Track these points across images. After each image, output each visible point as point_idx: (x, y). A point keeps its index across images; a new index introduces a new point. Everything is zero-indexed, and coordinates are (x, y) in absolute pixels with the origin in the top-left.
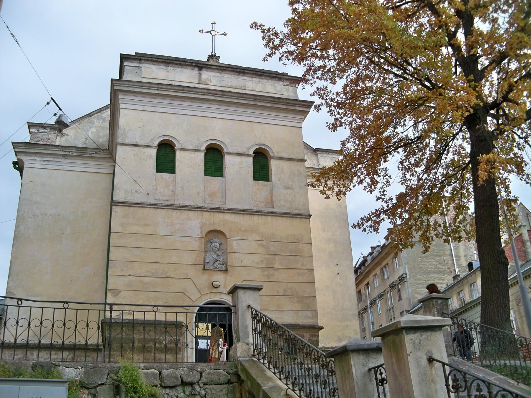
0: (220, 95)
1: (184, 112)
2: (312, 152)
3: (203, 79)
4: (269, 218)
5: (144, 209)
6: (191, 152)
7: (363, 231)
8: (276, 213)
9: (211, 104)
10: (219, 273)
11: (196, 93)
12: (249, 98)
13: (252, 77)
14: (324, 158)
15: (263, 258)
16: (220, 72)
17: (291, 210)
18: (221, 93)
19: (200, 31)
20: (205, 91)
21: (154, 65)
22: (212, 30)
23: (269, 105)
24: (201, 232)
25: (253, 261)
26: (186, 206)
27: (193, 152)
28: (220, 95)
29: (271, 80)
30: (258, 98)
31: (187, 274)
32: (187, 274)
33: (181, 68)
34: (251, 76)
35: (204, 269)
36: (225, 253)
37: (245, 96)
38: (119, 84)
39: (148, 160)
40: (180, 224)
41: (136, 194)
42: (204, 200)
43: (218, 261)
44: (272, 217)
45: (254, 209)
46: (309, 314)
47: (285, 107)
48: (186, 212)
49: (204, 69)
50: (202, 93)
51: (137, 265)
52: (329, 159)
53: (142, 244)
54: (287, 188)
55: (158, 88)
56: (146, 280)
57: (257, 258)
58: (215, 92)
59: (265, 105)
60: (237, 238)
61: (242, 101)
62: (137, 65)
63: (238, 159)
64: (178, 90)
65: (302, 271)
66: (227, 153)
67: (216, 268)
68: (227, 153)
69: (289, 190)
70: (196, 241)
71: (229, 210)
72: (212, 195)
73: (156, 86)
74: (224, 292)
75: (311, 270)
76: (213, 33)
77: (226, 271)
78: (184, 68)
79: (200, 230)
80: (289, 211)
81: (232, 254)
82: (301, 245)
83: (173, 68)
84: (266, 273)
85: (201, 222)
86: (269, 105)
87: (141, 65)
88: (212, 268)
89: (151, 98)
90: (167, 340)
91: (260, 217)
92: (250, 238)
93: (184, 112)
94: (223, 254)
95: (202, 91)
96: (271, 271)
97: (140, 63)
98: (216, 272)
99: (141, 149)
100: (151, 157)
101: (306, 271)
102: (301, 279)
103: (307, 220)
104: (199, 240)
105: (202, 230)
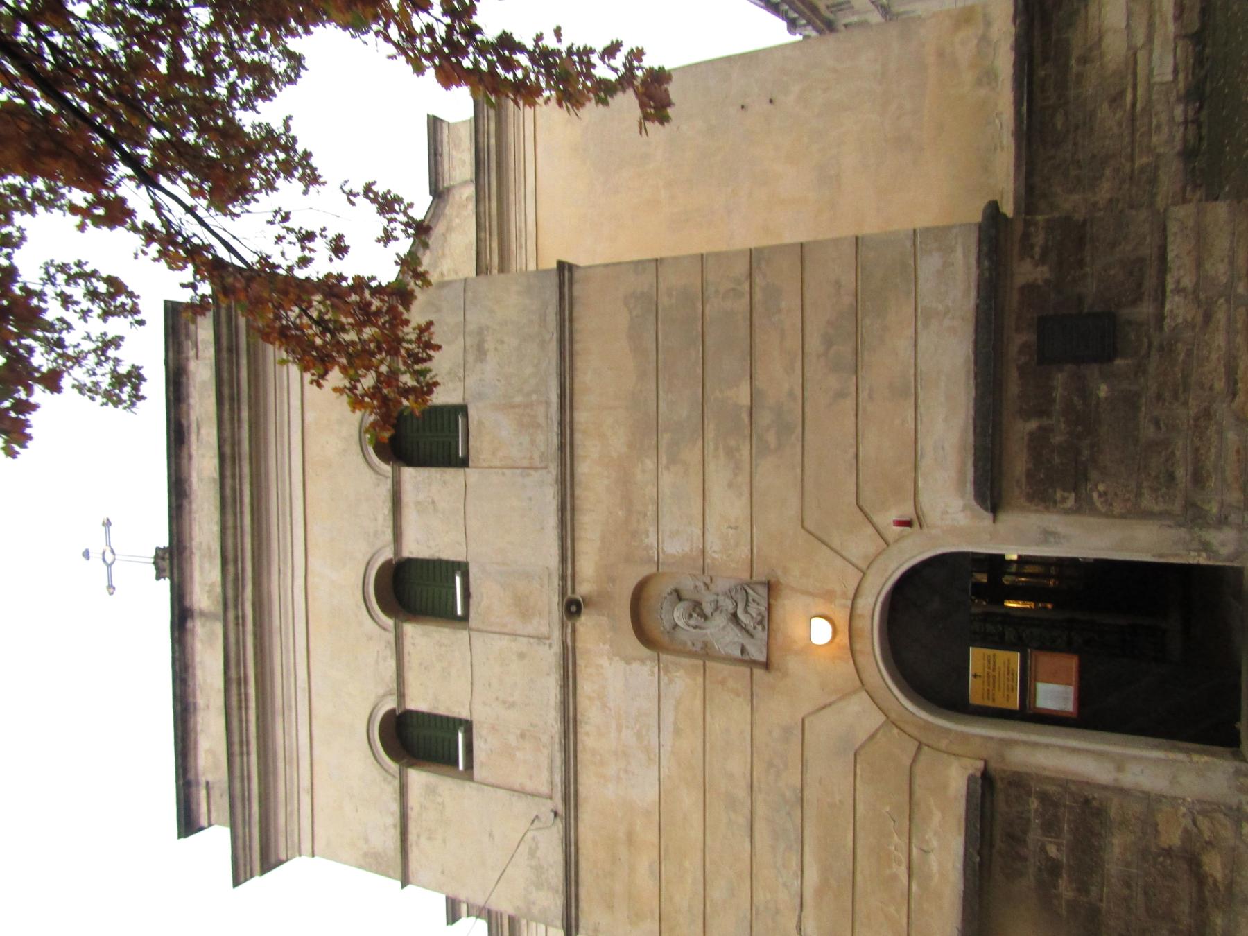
0: (236, 569)
1: (302, 674)
2: (442, 205)
3: (212, 609)
4: (582, 417)
5: (581, 839)
6: (406, 664)
7: (324, 183)
8: (562, 395)
9: (269, 593)
10: (778, 614)
11: (241, 644)
12: (233, 476)
13: (190, 457)
14: (454, 169)
15: (716, 448)
16: (187, 553)
17: (547, 337)
18: (231, 568)
19: (111, 594)
20: (231, 615)
21: (196, 743)
22: (104, 560)
23: (245, 414)
24: (643, 661)
25: (730, 485)
26: (564, 704)
27: (406, 658)
28: (236, 569)
29: (188, 396)
30: (228, 449)
31: (787, 730)
32: (787, 730)
33: (194, 668)
34: (185, 461)
35: (767, 666)
36: (708, 581)
37: (228, 492)
38: (245, 865)
39: (439, 800)
40: (619, 729)
41: (539, 854)
42: (540, 638)
43: (735, 615)
44: (575, 405)
45: (554, 472)
46: (929, 265)
47: (244, 361)
48: (583, 703)
49: (187, 603)
50: (237, 624)
51: (760, 896)
52: (454, 153)
53: (692, 864)
54: (481, 352)
55: (242, 754)
56: (812, 875)
57: (719, 473)
58: (230, 585)
59: (245, 426)
60: (652, 540)
61: (247, 499)
62: (203, 793)
63: (410, 517)
64: (239, 695)
65: (758, 296)
66: (397, 549)
67: (760, 623)
68: (397, 549)
69: (486, 346)
70: (671, 681)
71: (563, 560)
72: (524, 609)
73: (237, 760)
74: (849, 602)
75: (755, 257)
76: (109, 558)
77: (771, 588)
78: (193, 660)
79: (636, 665)
80: (553, 346)
81: (708, 561)
82: (664, 301)
83: (198, 692)
84: (771, 438)
85: (610, 659)
86: (245, 414)
87: (203, 780)
88: (760, 634)
89: (275, 768)
90: (860, 241)
91: (579, 452)
92: (650, 490)
93: (302, 674)
94: (712, 586)
95: (231, 626)
96: (765, 417)
97: (198, 784)
98: (774, 626)
99: (413, 814)
100: (431, 790)
101: (759, 280)
102: (790, 302)
103: (577, 275)
104: (667, 671)
105: (634, 659)
